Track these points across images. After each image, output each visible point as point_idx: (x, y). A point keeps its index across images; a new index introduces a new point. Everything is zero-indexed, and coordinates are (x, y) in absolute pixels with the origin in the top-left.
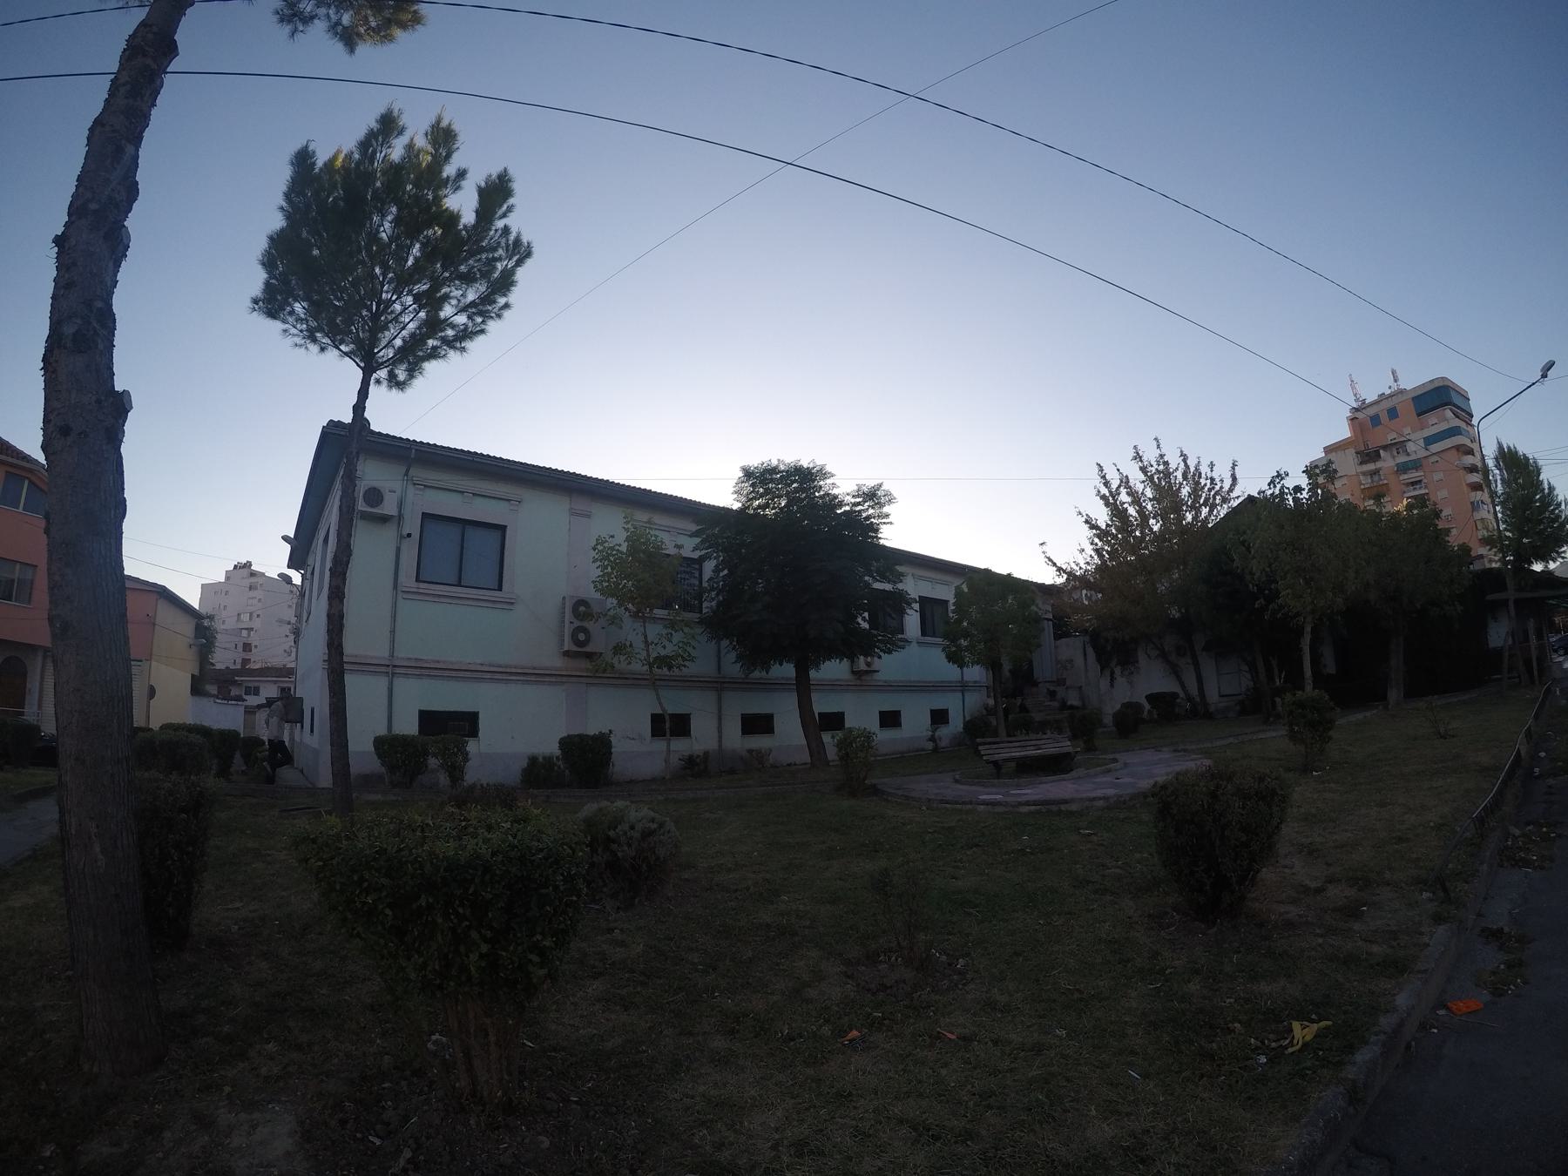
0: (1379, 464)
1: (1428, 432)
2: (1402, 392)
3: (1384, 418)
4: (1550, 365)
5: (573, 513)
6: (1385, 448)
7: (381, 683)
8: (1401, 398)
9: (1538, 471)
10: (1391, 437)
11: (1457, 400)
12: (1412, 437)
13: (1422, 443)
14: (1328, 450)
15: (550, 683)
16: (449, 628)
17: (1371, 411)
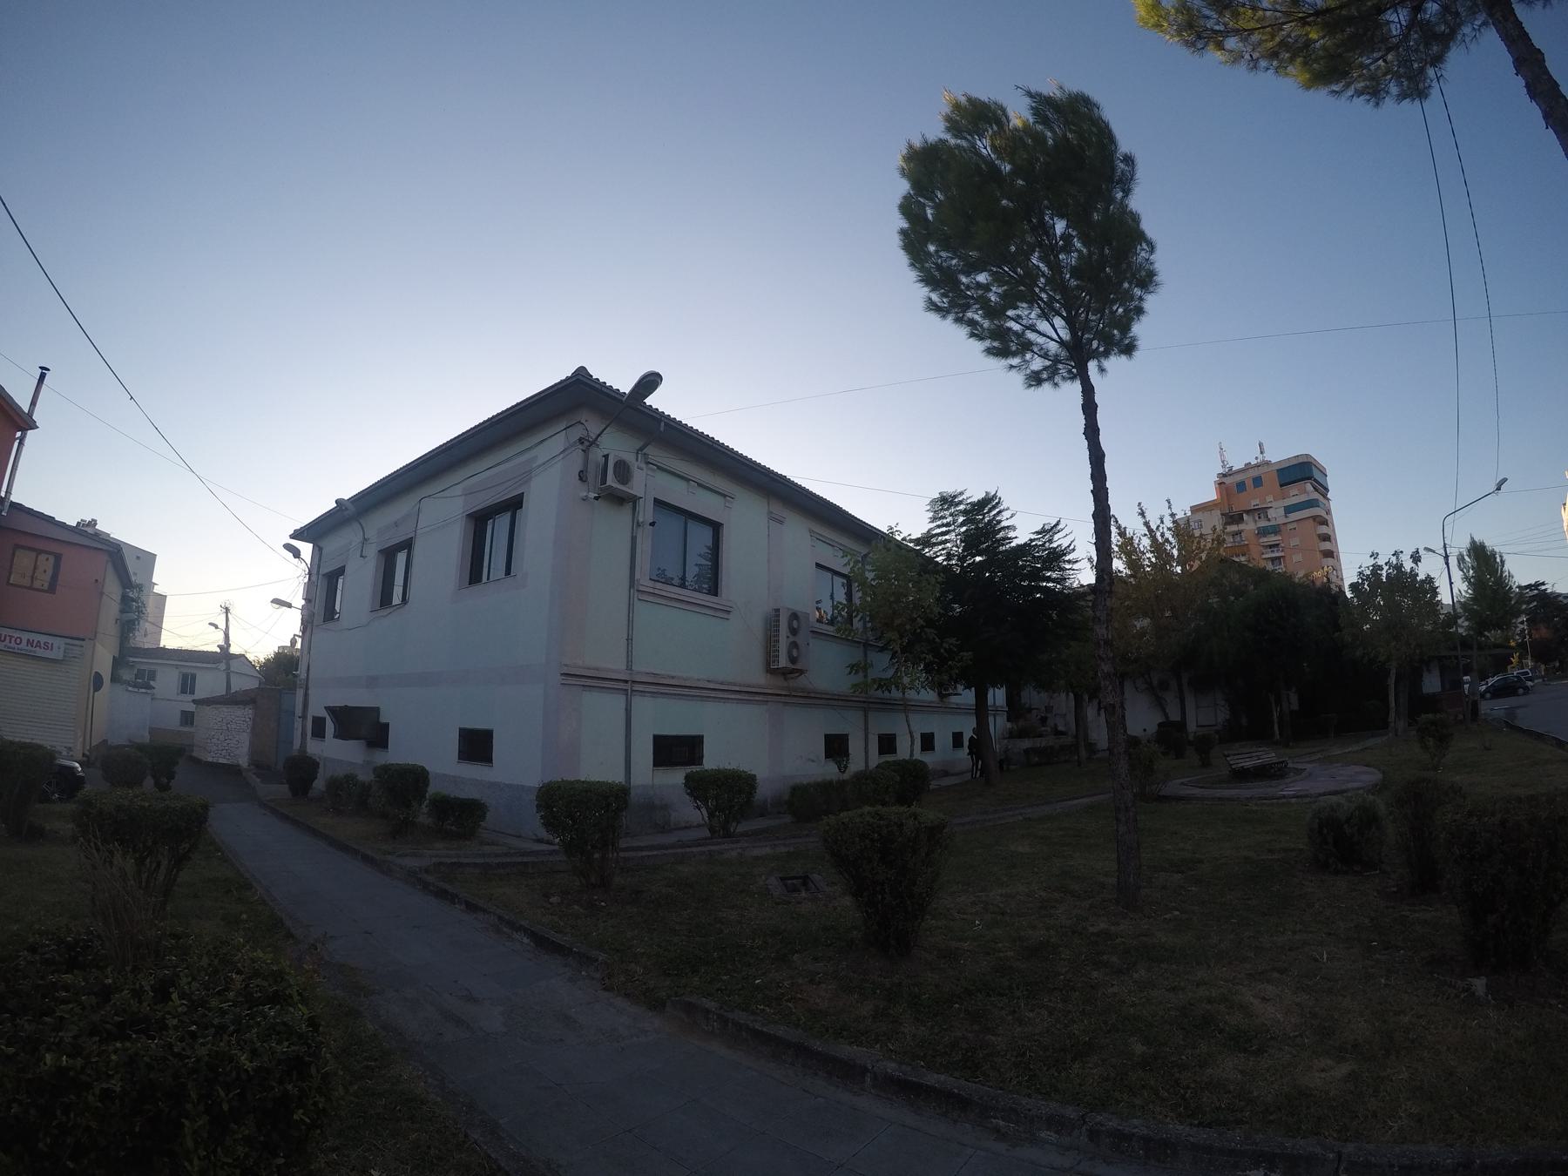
0: (1241, 527)
1: (1288, 502)
2: (1268, 463)
3: (1249, 484)
6: (1248, 512)
7: (619, 701)
8: (1265, 469)
10: (1254, 503)
11: (1317, 475)
13: (1282, 511)
16: (686, 641)
17: (1238, 478)
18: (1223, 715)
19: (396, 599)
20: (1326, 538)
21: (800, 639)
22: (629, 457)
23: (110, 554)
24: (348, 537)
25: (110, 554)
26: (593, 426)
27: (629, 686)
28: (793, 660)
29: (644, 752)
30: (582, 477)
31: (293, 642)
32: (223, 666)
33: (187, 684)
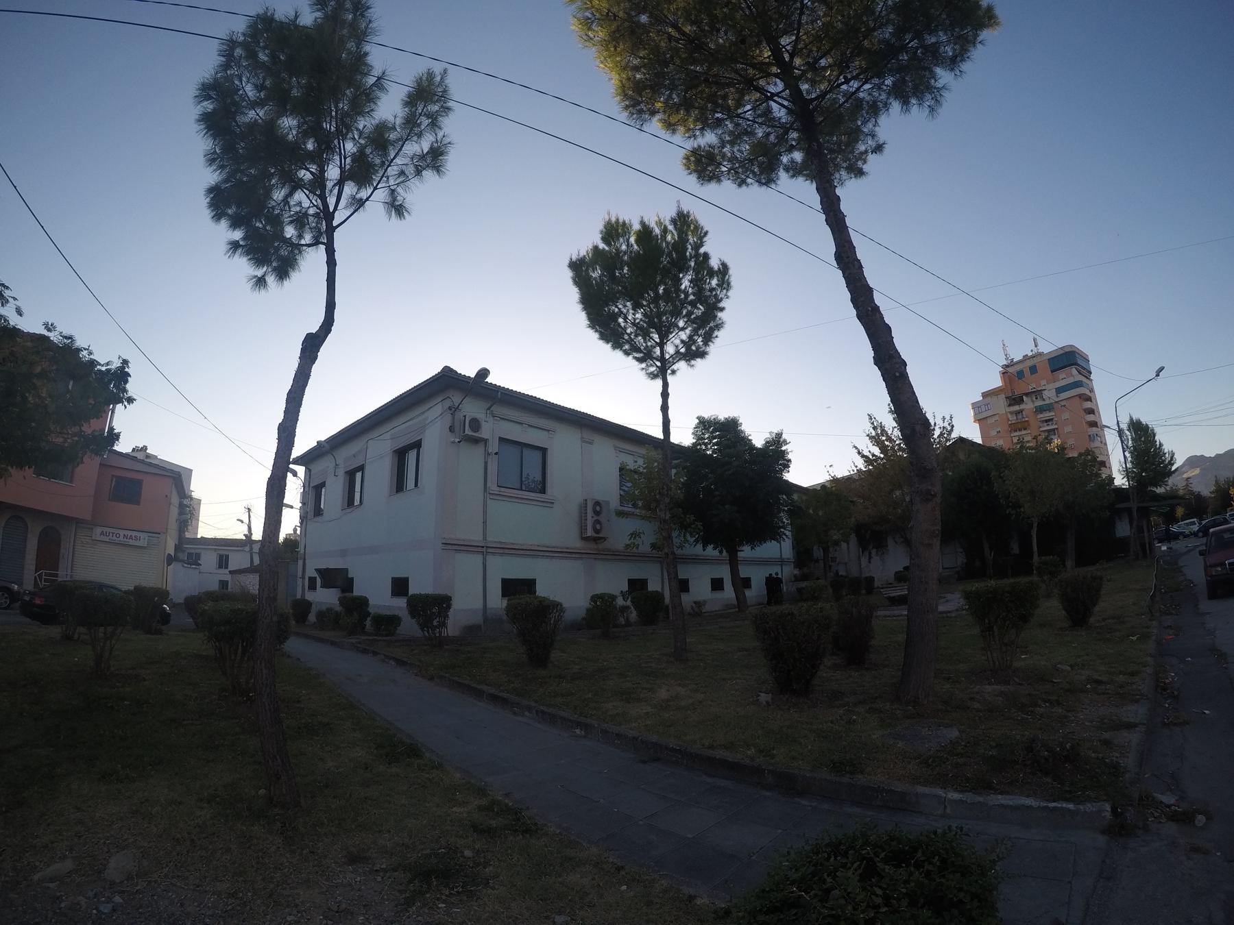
0: (1022, 407)
2: (1041, 354)
3: (1027, 372)
4: (1162, 369)
5: (583, 440)
6: (1027, 394)
7: (479, 558)
9: (1155, 435)
11: (1080, 362)
12: (1047, 387)
14: (985, 395)
15: (576, 559)
16: (518, 520)
17: (1018, 368)
18: (961, 559)
19: (357, 502)
20: (1091, 411)
21: (602, 518)
22: (481, 416)
23: (174, 478)
24: (326, 463)
25: (174, 478)
26: (456, 398)
27: (484, 550)
28: (597, 531)
29: (495, 589)
30: (451, 429)
31: (295, 530)
32: (247, 549)
33: (223, 562)
